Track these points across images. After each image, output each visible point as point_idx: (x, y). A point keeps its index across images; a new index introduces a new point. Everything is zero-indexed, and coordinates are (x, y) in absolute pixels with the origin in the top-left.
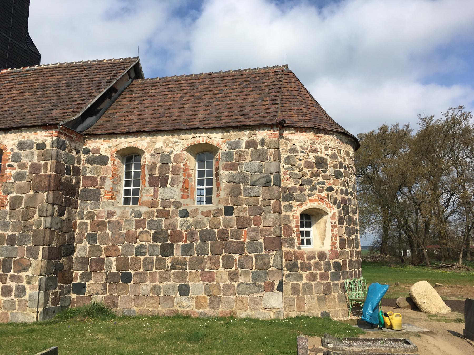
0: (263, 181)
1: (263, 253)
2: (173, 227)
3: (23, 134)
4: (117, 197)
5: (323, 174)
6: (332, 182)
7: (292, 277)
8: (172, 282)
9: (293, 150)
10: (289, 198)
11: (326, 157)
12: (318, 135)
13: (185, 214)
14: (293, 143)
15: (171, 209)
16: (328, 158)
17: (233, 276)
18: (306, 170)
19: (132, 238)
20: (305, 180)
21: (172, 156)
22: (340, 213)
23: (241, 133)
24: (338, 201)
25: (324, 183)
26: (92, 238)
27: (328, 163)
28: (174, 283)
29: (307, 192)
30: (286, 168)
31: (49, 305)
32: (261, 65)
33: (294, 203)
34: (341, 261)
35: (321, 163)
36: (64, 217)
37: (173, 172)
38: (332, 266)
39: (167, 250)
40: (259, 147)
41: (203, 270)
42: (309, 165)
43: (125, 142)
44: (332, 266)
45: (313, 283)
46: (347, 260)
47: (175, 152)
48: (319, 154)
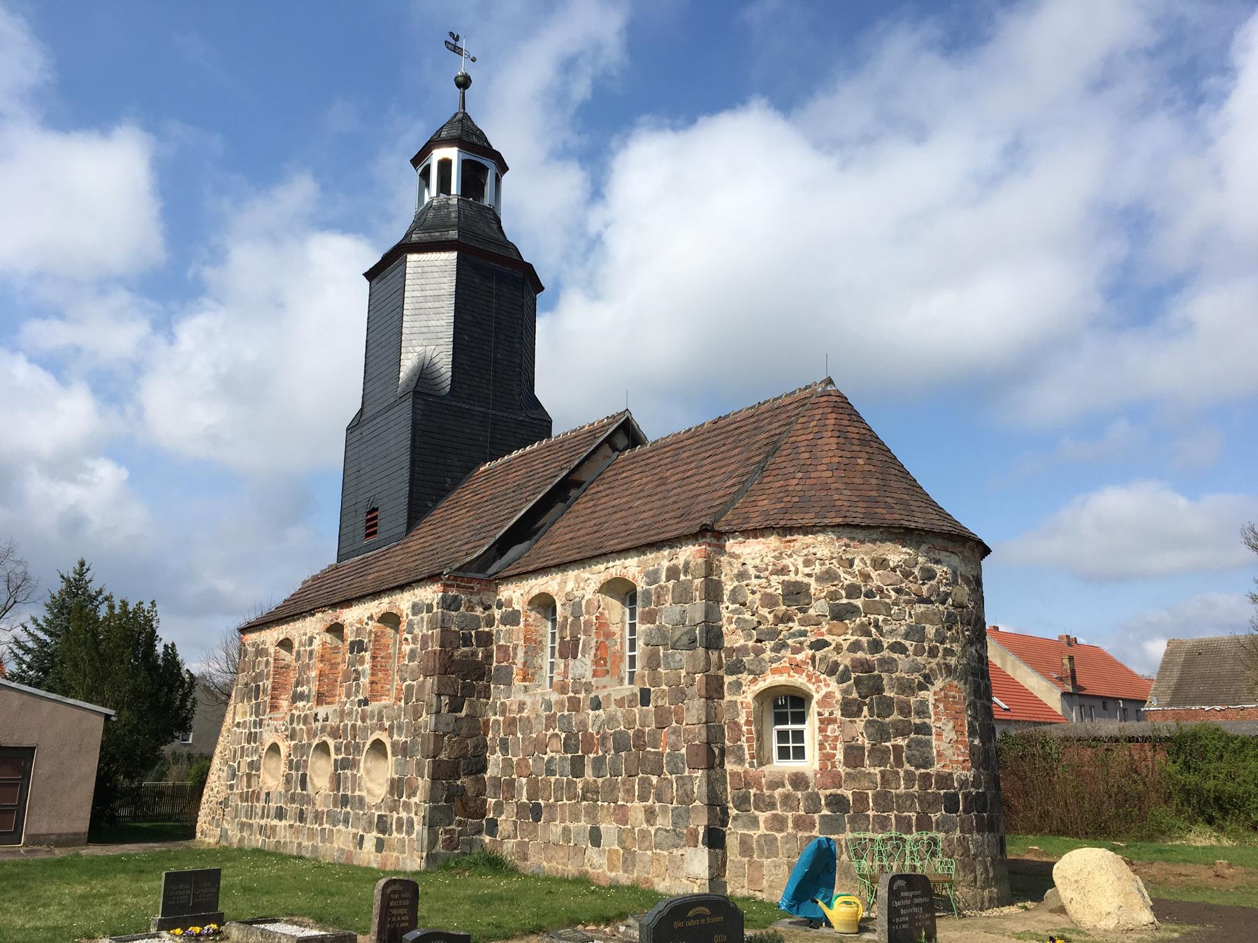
0: (685, 639)
1: (686, 774)
2: (583, 724)
3: (416, 591)
4: (537, 676)
5: (800, 615)
6: (824, 630)
7: (739, 822)
8: (583, 823)
9: (742, 575)
10: (736, 668)
11: (806, 580)
12: (789, 538)
13: (596, 705)
14: (742, 560)
15: (582, 696)
16: (812, 581)
17: (650, 814)
18: (764, 611)
19: (541, 746)
20: (762, 632)
21: (584, 603)
22: (846, 692)
23: (659, 554)
24: (841, 668)
25: (804, 634)
26: (504, 745)
27: (812, 591)
28: (584, 824)
29: (768, 655)
30: (731, 612)
31: (439, 848)
32: (767, 394)
33: (745, 677)
34: (849, 794)
35: (796, 594)
36: (463, 714)
37: (585, 632)
38: (823, 802)
39: (577, 768)
40: (682, 577)
41: (615, 803)
42: (769, 601)
43: (537, 585)
44: (823, 802)
45: (779, 836)
46: (870, 793)
47: (586, 598)
48: (792, 577)
